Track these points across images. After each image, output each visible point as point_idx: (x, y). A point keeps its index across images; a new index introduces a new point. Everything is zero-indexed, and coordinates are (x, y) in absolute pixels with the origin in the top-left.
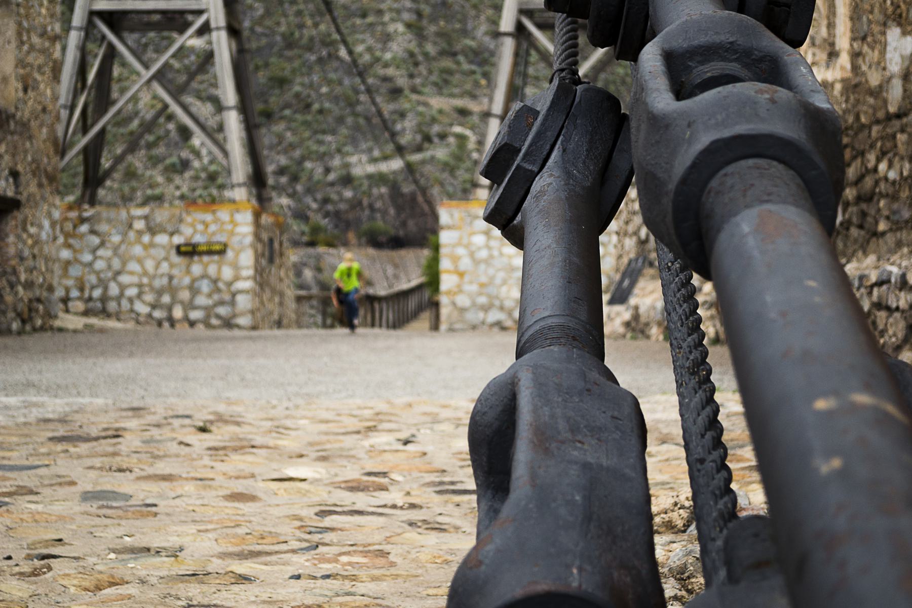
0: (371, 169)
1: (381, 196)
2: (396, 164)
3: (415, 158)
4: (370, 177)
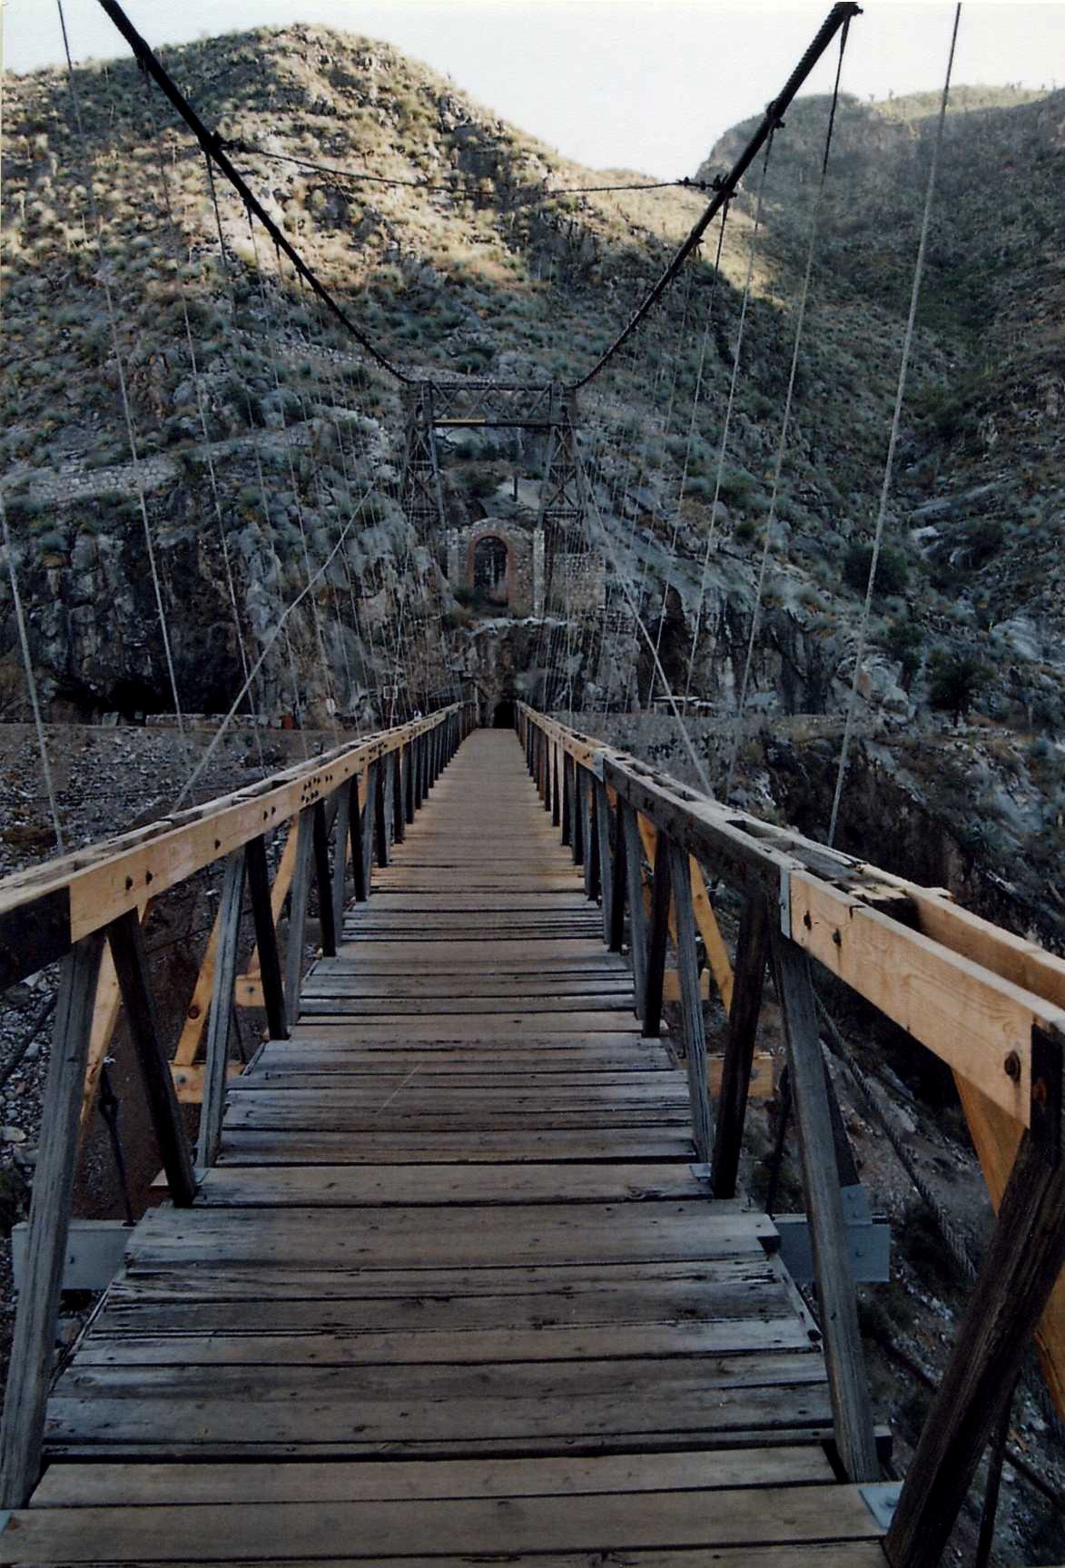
0: (84, 488)
1: (96, 561)
2: (157, 472)
3: (209, 452)
4: (81, 505)
